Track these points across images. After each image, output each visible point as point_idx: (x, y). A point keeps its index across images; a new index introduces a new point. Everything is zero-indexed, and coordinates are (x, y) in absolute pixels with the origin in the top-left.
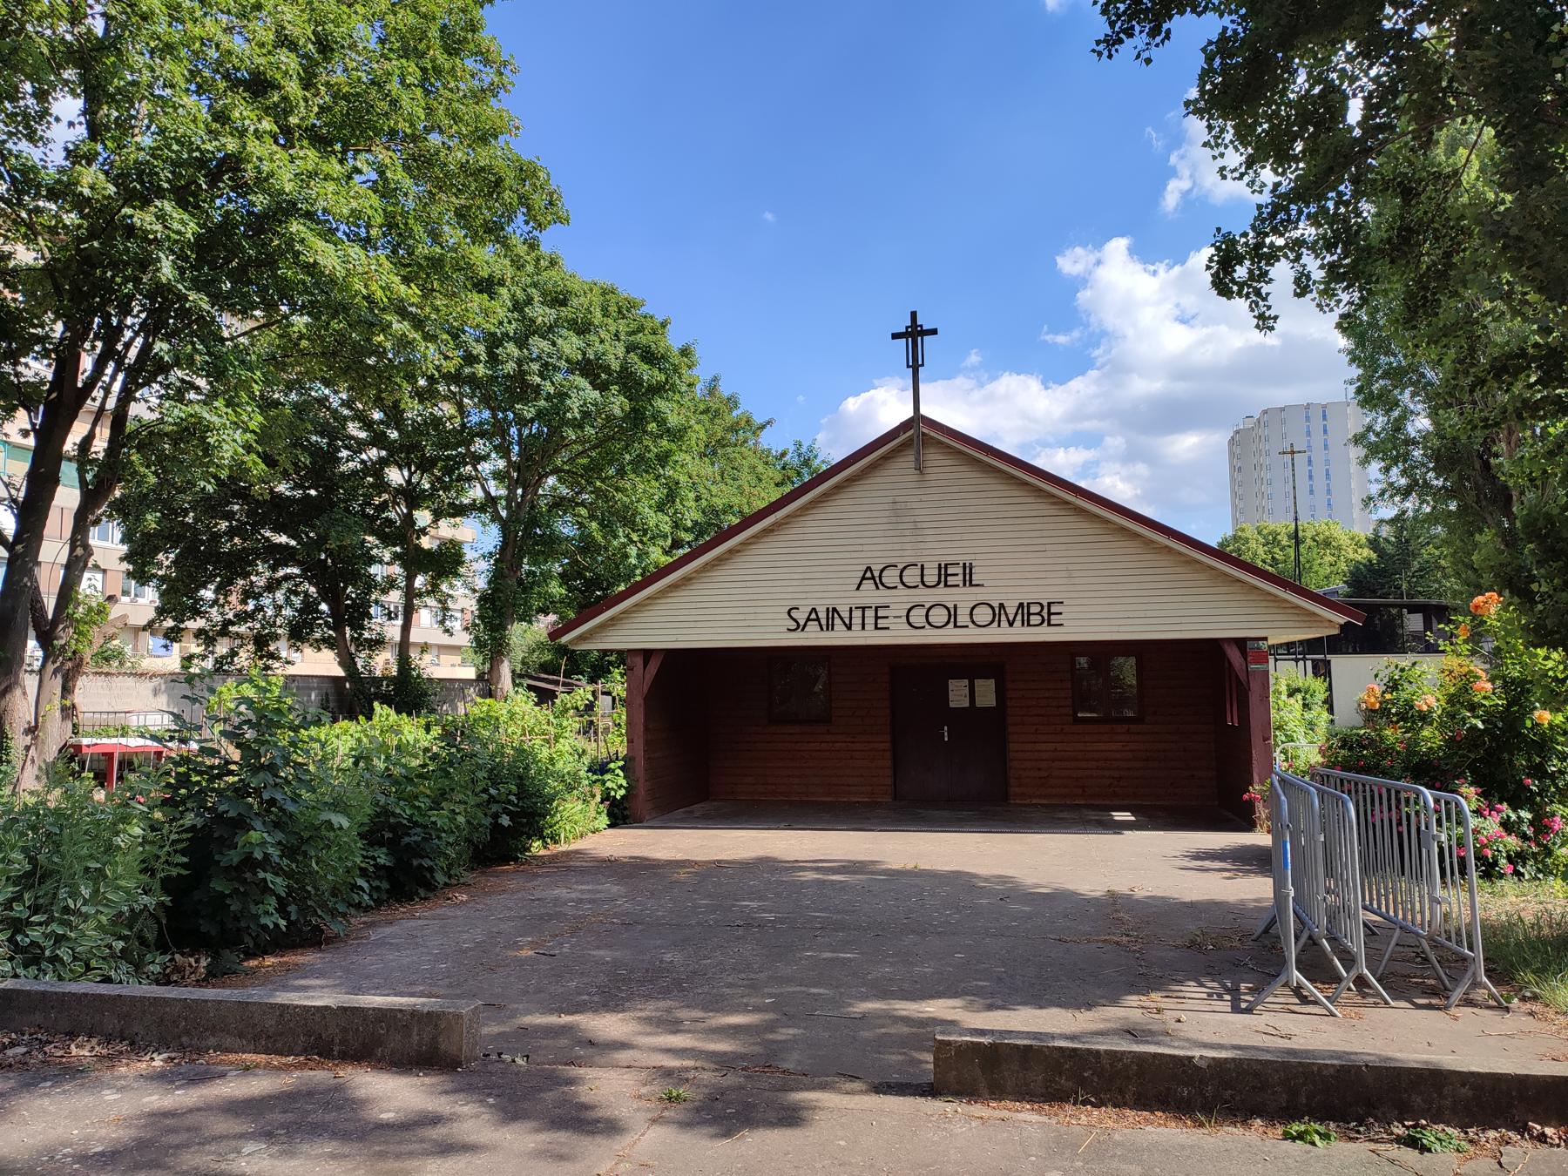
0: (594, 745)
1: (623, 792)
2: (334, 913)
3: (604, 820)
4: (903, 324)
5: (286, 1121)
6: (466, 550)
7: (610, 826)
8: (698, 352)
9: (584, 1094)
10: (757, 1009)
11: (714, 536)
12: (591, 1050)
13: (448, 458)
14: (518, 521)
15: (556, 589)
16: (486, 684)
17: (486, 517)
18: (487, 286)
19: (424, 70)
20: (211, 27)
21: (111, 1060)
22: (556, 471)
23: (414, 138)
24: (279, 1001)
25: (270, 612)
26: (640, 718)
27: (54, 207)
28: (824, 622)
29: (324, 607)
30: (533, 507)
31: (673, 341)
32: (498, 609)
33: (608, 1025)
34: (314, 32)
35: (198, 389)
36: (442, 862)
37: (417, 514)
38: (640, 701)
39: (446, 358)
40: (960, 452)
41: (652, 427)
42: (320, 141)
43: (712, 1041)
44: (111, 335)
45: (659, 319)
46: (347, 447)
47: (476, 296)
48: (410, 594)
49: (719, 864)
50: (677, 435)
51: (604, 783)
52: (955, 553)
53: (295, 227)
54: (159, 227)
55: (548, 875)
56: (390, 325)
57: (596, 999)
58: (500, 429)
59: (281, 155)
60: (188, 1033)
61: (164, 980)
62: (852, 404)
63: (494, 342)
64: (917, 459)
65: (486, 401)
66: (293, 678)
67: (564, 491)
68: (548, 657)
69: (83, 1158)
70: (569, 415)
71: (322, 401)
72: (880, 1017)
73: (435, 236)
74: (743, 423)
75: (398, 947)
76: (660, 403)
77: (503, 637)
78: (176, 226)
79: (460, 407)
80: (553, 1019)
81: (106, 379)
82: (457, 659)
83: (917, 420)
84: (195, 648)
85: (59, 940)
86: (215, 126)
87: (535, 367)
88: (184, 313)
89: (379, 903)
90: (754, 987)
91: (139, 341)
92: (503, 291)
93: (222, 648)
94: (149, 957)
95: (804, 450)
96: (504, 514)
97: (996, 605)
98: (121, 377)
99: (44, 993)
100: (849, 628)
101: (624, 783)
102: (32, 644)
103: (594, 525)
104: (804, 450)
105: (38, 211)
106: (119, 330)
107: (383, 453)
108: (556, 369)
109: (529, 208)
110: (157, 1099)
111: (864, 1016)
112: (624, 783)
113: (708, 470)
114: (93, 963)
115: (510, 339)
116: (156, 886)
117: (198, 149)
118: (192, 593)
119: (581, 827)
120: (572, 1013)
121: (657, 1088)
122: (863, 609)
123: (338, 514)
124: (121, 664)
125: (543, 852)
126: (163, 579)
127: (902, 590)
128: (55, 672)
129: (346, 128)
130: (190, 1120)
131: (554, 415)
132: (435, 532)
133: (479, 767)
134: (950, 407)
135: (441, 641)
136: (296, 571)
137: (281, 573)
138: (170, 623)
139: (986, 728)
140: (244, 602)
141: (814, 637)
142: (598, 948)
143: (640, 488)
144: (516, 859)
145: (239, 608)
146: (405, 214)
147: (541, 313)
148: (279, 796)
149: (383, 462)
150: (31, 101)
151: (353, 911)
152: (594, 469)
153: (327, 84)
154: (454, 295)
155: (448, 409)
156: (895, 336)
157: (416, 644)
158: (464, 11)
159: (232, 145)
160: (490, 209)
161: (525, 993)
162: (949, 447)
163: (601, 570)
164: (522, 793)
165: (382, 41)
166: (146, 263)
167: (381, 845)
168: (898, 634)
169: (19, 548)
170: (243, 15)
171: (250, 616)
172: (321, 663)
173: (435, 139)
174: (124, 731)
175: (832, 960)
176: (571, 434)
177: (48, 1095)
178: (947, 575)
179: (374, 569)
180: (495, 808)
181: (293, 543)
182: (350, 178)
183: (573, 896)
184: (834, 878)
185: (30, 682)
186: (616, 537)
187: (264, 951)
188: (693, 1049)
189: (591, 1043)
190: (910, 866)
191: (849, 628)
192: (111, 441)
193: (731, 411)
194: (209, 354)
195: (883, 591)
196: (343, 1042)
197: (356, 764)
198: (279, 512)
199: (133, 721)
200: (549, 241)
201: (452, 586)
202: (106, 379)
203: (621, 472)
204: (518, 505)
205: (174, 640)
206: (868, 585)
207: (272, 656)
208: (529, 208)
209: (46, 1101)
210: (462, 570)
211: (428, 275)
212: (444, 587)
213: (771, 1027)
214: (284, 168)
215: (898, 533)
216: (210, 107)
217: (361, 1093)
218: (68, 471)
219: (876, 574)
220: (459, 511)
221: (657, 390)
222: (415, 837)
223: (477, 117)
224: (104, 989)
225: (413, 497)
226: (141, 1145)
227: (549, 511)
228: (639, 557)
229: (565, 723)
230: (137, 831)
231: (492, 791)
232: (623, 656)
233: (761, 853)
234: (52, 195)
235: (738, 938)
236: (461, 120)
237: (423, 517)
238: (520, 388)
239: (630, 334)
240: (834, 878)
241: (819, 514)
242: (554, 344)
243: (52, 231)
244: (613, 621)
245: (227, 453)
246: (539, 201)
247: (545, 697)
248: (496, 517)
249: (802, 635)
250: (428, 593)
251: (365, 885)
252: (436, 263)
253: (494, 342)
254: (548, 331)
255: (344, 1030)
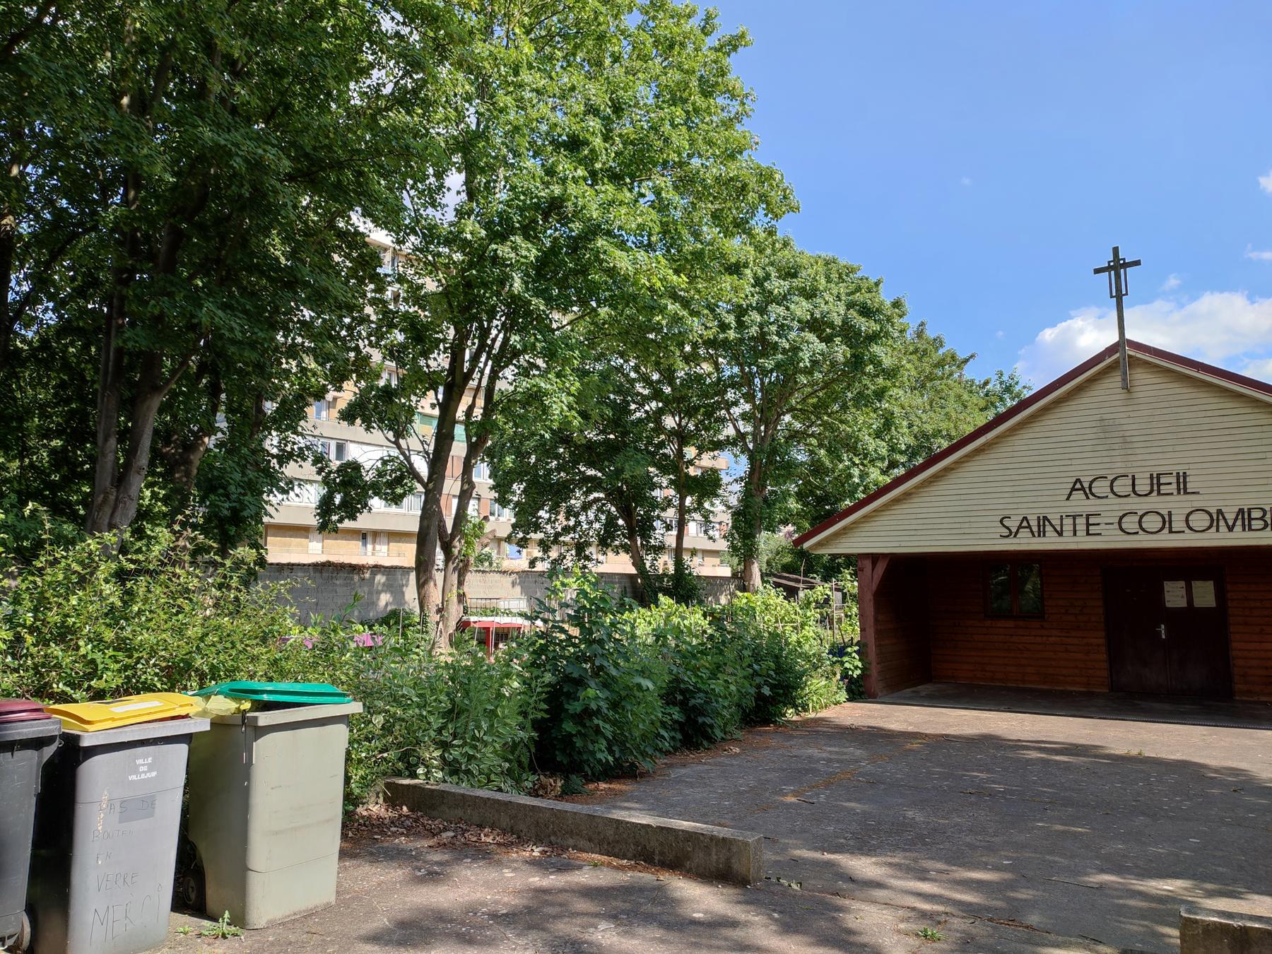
0: (830, 632)
1: (859, 672)
2: (644, 754)
3: (843, 696)
4: (1106, 259)
5: (631, 908)
6: (723, 475)
7: (849, 700)
8: (908, 306)
9: (850, 921)
10: (996, 868)
11: (928, 460)
12: (851, 886)
13: (706, 406)
14: (762, 451)
15: (793, 505)
16: (741, 580)
17: (737, 450)
18: (735, 269)
19: (687, 112)
20: (544, 110)
21: (507, 845)
22: (791, 410)
23: (681, 164)
24: (615, 817)
25: (585, 526)
26: (870, 610)
27: (447, 250)
28: (1035, 529)
29: (621, 522)
30: (773, 440)
31: (885, 297)
32: (748, 522)
33: (864, 866)
34: (610, 99)
35: (538, 368)
36: (720, 722)
37: (685, 450)
38: (869, 596)
39: (707, 328)
40: (1241, 396)
41: (870, 368)
42: (615, 178)
43: (957, 891)
44: (485, 333)
45: (873, 280)
46: (634, 402)
47: (728, 278)
48: (683, 511)
49: (947, 738)
50: (891, 374)
51: (842, 663)
52: (1170, 464)
53: (600, 242)
54: (513, 255)
55: (802, 737)
56: (666, 307)
57: (851, 843)
58: (747, 379)
59: (590, 192)
60: (555, 834)
61: (534, 793)
62: (1048, 335)
63: (740, 312)
64: (1124, 380)
65: (736, 359)
66: (602, 575)
67: (798, 425)
68: (788, 559)
69: (494, 916)
70: (801, 365)
71: (619, 369)
72: (1116, 890)
73: (697, 235)
74: (949, 359)
75: (691, 785)
76: (876, 349)
77: (753, 544)
78: (524, 253)
79: (716, 365)
80: (817, 855)
81: (481, 365)
82: (717, 561)
83: (1122, 343)
84: (537, 552)
85: (470, 758)
86: (546, 178)
87: (774, 328)
88: (529, 313)
89: (676, 749)
90: (991, 849)
91: (501, 335)
92: (748, 271)
93: (554, 554)
94: (524, 776)
95: (1005, 378)
96: (751, 446)
97: (1213, 511)
98: (490, 363)
99: (463, 795)
100: (1060, 534)
101: (860, 665)
102: (438, 550)
103: (822, 452)
104: (1005, 378)
105: (439, 255)
106: (489, 328)
107: (660, 405)
108: (790, 328)
109: (768, 204)
110: (537, 880)
111: (1101, 887)
112: (860, 665)
113: (920, 400)
114: (493, 777)
115: (753, 308)
116: (529, 725)
117: (536, 197)
118: (534, 514)
119: (827, 701)
120: (833, 853)
121: (918, 927)
122: (1074, 517)
123: (631, 452)
124: (491, 564)
125: (795, 718)
126: (517, 504)
127: (1113, 500)
128: (454, 569)
129: (633, 165)
130: (562, 898)
131: (789, 367)
132: (700, 462)
133: (744, 647)
134: (1152, 328)
135: (705, 543)
136: (602, 495)
137: (591, 497)
138: (521, 535)
139: (1202, 630)
140: (567, 519)
141: (1025, 542)
142: (849, 800)
143: (861, 420)
144: (775, 722)
145: (565, 523)
146: (675, 222)
147: (777, 286)
148: (606, 664)
149: (660, 412)
150: (432, 180)
151: (658, 754)
152: (821, 407)
153: (620, 135)
154: (712, 278)
155: (706, 367)
156: (1097, 271)
157: (687, 550)
158: (715, 62)
159: (557, 190)
160: (737, 209)
161: (793, 832)
162: (1157, 366)
163: (829, 489)
164: (779, 669)
165: (657, 97)
166: (504, 280)
167: (674, 704)
168: (1109, 539)
169: (431, 485)
170: (563, 97)
171: (574, 529)
172: (619, 563)
173: (696, 162)
174: (495, 612)
175: (1063, 832)
176: (803, 379)
177: (469, 868)
178: (1159, 484)
179: (656, 493)
180: (758, 680)
181: (600, 474)
182: (636, 201)
183: (824, 755)
184: (1058, 758)
185: (439, 577)
186: (841, 461)
187: (597, 778)
188: (941, 896)
189: (852, 880)
190: (1134, 752)
191: (1060, 534)
192: (485, 409)
193: (937, 349)
194: (545, 341)
195: (1093, 500)
196: (662, 853)
197: (657, 641)
198: (591, 453)
199: (502, 605)
200: (786, 227)
201: (712, 505)
202: (481, 365)
203: (844, 407)
204: (763, 439)
205: (522, 547)
206: (1078, 495)
207: (588, 558)
208: (768, 204)
209: (469, 873)
210: (720, 492)
211: (692, 267)
212: (707, 505)
213: (1010, 885)
214: (590, 200)
215: (1106, 447)
216: (543, 165)
217: (677, 894)
218: (459, 431)
219: (1086, 485)
220: (718, 446)
221: (873, 338)
222: (697, 701)
223: (727, 140)
224: (499, 796)
225: (682, 437)
226: (530, 911)
227: (786, 442)
228: (861, 477)
229: (809, 614)
230: (516, 685)
231: (756, 667)
232: (852, 560)
233: (984, 731)
234: (447, 242)
235: (971, 804)
236: (715, 144)
237: (690, 452)
238: (763, 345)
239: (848, 294)
240: (1058, 758)
241: (1027, 434)
242: (788, 309)
243: (447, 266)
244: (845, 530)
245: (556, 410)
246: (776, 196)
247: (791, 593)
248: (745, 449)
249: (1015, 541)
250: (695, 510)
251: (666, 735)
252: (698, 256)
253: (740, 312)
254: (782, 300)
255: (661, 844)
